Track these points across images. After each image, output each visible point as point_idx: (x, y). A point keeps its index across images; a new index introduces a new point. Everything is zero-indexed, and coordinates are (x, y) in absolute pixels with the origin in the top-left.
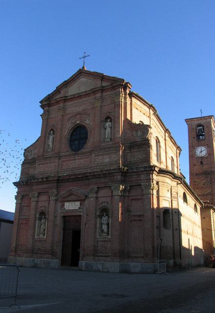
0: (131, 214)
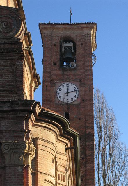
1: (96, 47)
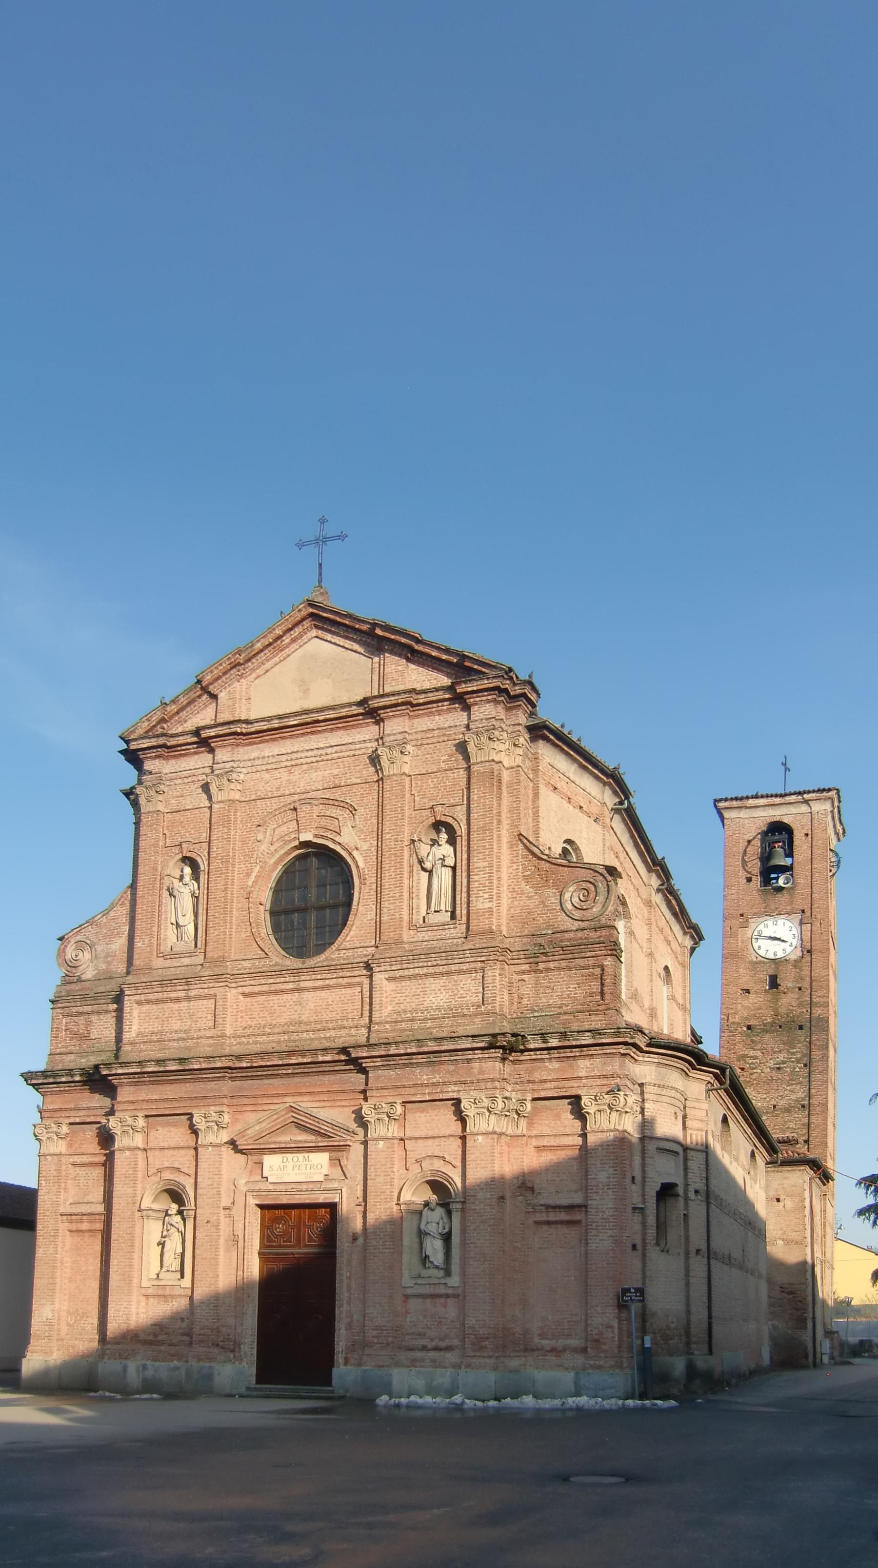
0: (535, 1201)
1: (844, 832)
